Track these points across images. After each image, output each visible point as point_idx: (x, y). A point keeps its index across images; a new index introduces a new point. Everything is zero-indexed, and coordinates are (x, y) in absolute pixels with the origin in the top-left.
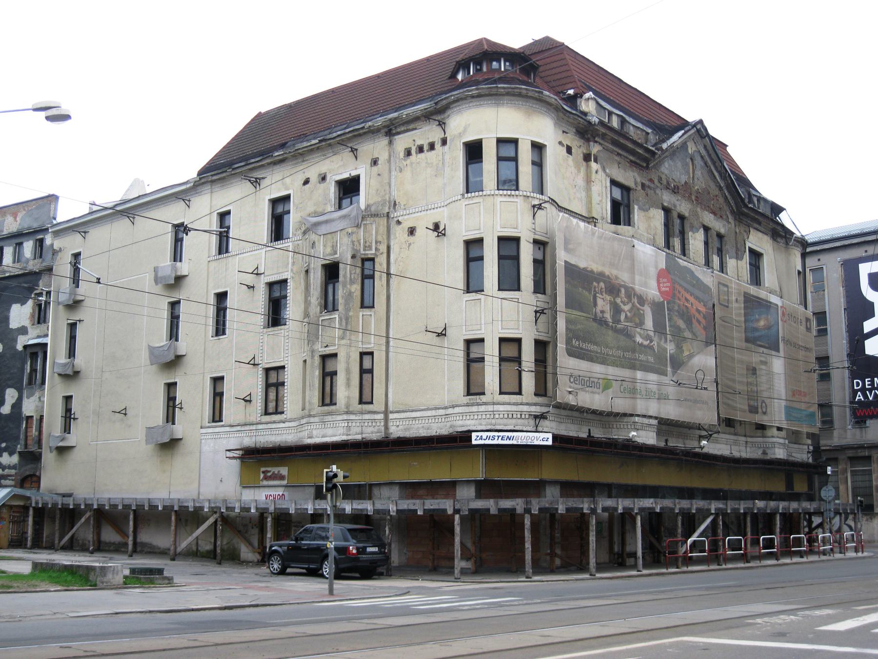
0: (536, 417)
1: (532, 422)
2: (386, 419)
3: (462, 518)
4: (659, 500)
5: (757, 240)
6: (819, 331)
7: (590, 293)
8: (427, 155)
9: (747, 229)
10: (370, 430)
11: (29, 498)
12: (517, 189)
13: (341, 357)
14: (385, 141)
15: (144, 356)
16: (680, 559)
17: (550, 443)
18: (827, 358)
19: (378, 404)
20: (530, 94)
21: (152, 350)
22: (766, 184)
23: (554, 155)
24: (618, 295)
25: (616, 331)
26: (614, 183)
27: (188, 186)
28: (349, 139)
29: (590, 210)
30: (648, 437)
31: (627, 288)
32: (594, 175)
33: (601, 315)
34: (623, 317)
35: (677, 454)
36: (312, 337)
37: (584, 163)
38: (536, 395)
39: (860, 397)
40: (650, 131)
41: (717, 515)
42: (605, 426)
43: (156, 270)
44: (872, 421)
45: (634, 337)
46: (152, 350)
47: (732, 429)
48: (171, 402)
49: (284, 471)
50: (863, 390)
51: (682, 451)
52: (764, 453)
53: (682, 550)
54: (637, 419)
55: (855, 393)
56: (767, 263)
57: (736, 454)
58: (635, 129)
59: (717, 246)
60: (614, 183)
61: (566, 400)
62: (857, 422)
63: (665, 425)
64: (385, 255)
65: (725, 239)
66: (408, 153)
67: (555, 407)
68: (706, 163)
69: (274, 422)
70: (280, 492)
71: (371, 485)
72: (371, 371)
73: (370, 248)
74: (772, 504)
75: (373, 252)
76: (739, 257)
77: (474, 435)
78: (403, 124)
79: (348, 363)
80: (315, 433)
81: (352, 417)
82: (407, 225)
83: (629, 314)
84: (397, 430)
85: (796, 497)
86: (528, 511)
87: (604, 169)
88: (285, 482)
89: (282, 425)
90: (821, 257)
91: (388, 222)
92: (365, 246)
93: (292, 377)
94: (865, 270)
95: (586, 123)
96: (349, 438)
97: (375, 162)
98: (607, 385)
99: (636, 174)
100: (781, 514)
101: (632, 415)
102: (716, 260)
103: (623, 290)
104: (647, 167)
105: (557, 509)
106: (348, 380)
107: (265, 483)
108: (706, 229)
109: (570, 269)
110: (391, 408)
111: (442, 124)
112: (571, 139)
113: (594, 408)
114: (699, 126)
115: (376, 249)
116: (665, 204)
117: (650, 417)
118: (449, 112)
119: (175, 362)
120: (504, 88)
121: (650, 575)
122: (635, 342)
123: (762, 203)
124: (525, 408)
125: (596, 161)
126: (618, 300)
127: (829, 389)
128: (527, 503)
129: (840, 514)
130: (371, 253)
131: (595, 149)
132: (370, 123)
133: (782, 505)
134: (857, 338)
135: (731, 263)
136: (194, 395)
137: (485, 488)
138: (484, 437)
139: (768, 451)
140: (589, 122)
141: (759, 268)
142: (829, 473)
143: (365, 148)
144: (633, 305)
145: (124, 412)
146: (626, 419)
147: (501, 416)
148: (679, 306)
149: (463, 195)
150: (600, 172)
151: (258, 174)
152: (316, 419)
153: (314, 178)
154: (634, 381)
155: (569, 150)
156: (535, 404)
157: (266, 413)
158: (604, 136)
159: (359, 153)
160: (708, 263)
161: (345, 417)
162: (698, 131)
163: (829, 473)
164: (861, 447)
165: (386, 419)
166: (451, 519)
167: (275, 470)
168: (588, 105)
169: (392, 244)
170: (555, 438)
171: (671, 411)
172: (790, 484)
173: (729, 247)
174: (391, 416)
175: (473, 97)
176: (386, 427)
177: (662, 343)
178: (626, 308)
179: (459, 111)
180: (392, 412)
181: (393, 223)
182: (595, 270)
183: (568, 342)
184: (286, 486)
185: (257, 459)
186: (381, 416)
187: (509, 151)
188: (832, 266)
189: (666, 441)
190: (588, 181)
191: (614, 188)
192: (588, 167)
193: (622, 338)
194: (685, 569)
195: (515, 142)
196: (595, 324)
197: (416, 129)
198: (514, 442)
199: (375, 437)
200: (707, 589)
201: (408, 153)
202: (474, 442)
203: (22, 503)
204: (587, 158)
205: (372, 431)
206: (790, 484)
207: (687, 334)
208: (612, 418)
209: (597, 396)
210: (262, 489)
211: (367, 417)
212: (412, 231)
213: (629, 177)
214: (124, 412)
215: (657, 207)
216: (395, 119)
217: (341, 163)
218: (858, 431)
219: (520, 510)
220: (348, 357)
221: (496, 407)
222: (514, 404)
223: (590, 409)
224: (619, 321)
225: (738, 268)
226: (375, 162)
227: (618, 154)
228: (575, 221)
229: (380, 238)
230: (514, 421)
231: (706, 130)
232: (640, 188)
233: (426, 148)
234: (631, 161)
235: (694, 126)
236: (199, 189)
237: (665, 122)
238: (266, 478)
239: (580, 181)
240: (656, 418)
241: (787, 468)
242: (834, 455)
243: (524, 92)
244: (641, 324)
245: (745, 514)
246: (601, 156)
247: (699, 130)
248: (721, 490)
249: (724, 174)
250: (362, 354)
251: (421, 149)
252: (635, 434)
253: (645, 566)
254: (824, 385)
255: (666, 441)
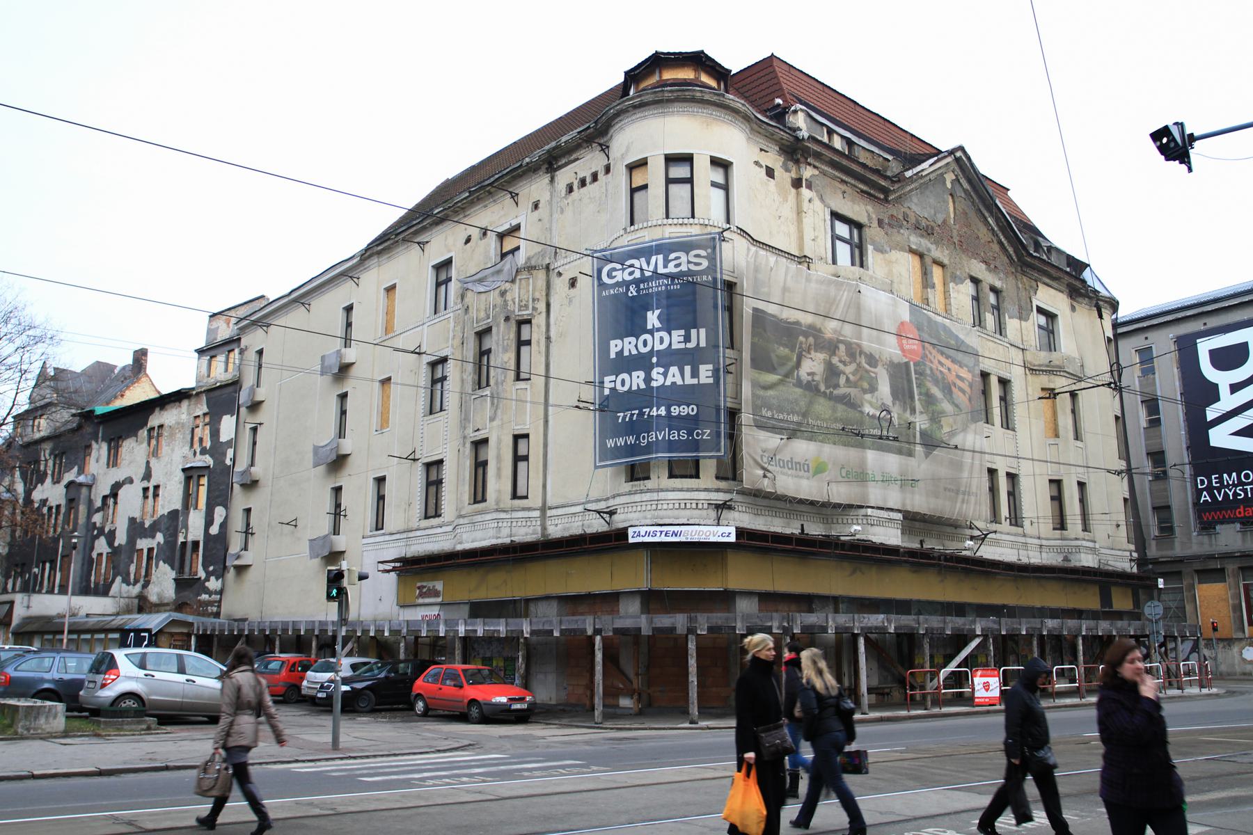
0: (718, 507)
1: (713, 514)
2: (543, 516)
3: (603, 639)
4: (893, 617)
5: (1049, 297)
6: (1150, 422)
7: (792, 350)
8: (590, 187)
9: (1034, 284)
10: (523, 531)
11: (192, 624)
12: (693, 217)
13: (492, 443)
14: (546, 179)
15: (309, 457)
16: (929, 698)
17: (733, 539)
18: (1162, 452)
19: (535, 500)
20: (707, 97)
21: (316, 449)
22: (1061, 233)
23: (746, 175)
24: (834, 354)
25: (831, 397)
26: (836, 216)
27: (355, 261)
28: (509, 182)
29: (801, 246)
30: (890, 535)
31: (848, 345)
32: (805, 205)
33: (810, 378)
34: (842, 380)
35: (933, 558)
36: (465, 420)
37: (793, 191)
38: (717, 478)
39: (1205, 497)
40: (890, 158)
41: (985, 636)
42: (826, 521)
43: (323, 358)
44: (1224, 526)
45: (861, 405)
46: (316, 449)
47: (1019, 530)
48: (337, 512)
49: (439, 586)
50: (1210, 489)
51: (942, 554)
52: (1066, 559)
53: (930, 687)
54: (869, 511)
55: (1199, 493)
56: (1062, 325)
57: (1025, 560)
58: (867, 152)
59: (991, 306)
60: (836, 216)
61: (757, 486)
62: (1203, 529)
63: (912, 521)
64: (544, 315)
65: (1004, 294)
66: (570, 189)
67: (742, 492)
68: (973, 203)
69: (432, 527)
70: (434, 611)
71: (528, 601)
72: (526, 458)
73: (526, 307)
74: (1071, 623)
75: (530, 311)
76: (1022, 317)
77: (631, 531)
78: (563, 155)
79: (499, 449)
80: (465, 536)
81: (503, 515)
82: (567, 276)
83: (851, 377)
84: (558, 529)
85: (1119, 615)
86: (691, 630)
87: (821, 199)
88: (439, 600)
89: (439, 530)
90: (1150, 335)
91: (548, 275)
92: (520, 306)
93: (448, 473)
94: (1204, 347)
95: (791, 139)
96: (499, 541)
97: (536, 206)
98: (820, 469)
99: (870, 208)
100: (1084, 638)
101: (861, 507)
102: (990, 319)
103: (842, 347)
104: (886, 200)
105: (734, 628)
106: (499, 469)
107: (421, 601)
108: (976, 281)
109: (758, 315)
110: (549, 503)
111: (605, 148)
112: (774, 159)
113: (802, 497)
114: (959, 154)
115: (534, 309)
116: (914, 247)
117: (891, 510)
118: (612, 131)
119: (338, 462)
120: (671, 91)
121: (881, 720)
122: (862, 412)
123: (1054, 253)
124: (703, 495)
125: (809, 187)
126: (835, 360)
127: (1165, 490)
128: (691, 619)
129: (1175, 638)
130: (525, 314)
131: (808, 172)
132: (527, 160)
133: (1085, 626)
134: (1198, 428)
135: (1012, 325)
136: (358, 500)
137: (652, 600)
138: (643, 533)
139: (1071, 557)
140: (797, 138)
141: (1053, 332)
142: (1161, 586)
143: (526, 191)
144: (859, 365)
145: (294, 524)
146: (853, 512)
147: (671, 506)
148: (931, 369)
149: (625, 229)
150: (817, 202)
151: (420, 239)
152: (466, 521)
153: (475, 233)
154: (863, 463)
155: (770, 173)
156: (718, 490)
157: (426, 517)
158: (818, 156)
159: (521, 199)
160: (979, 322)
161: (495, 515)
162: (958, 160)
163: (1161, 586)
164: (1211, 557)
165: (543, 516)
166: (591, 640)
167: (430, 584)
168: (799, 120)
169: (552, 301)
170: (740, 532)
171: (920, 503)
172: (1106, 599)
173: (1010, 306)
174: (549, 513)
175: (635, 107)
176: (544, 528)
177: (908, 414)
178: (849, 369)
179: (621, 128)
180: (550, 508)
181: (553, 276)
182: (803, 322)
183: (756, 410)
184: (441, 604)
185: (414, 569)
186: (537, 514)
187: (680, 171)
188: (1163, 342)
189: (922, 542)
190: (799, 212)
191: (838, 224)
192: (798, 194)
193: (840, 407)
194: (936, 710)
195: (688, 159)
196: (799, 391)
197: (577, 159)
198: (683, 539)
199: (529, 539)
200: (408, 784)
201: (570, 189)
202: (631, 540)
203: (185, 631)
204: (797, 183)
205: (526, 532)
206: (1106, 599)
207: (946, 406)
208: (829, 511)
209: (805, 483)
210: (418, 608)
211: (520, 514)
212: (573, 283)
213: (859, 210)
214: (294, 524)
215: (902, 249)
216: (554, 149)
217: (502, 213)
218: (1205, 539)
219: (681, 629)
220: (499, 441)
221: (662, 495)
222: (688, 490)
223: (795, 498)
224: (837, 386)
225: (1024, 330)
226: (536, 206)
227: (843, 181)
228: (762, 252)
229: (537, 295)
230: (688, 513)
231: (969, 158)
232: (875, 224)
233: (588, 180)
234: (862, 191)
235: (951, 152)
236: (368, 263)
237: (914, 152)
238: (422, 595)
239: (788, 210)
240: (899, 511)
241: (1102, 579)
242: (1174, 569)
243: (698, 94)
244: (873, 389)
245: (1029, 636)
246: (816, 182)
247: (961, 160)
248: (1004, 606)
249: (1005, 227)
250: (517, 438)
251: (583, 183)
252: (859, 528)
253: (872, 707)
254: (1159, 485)
255: (922, 542)
